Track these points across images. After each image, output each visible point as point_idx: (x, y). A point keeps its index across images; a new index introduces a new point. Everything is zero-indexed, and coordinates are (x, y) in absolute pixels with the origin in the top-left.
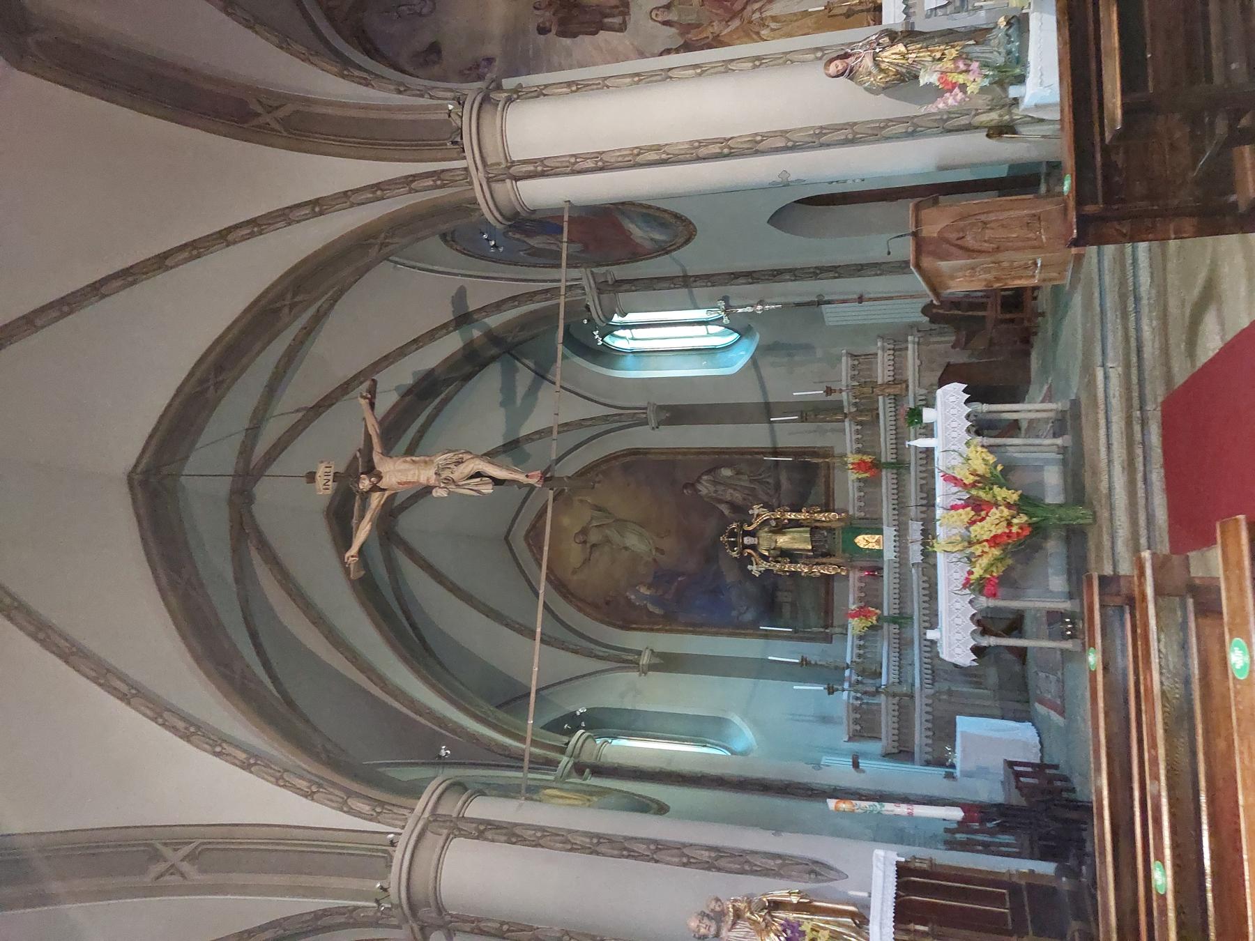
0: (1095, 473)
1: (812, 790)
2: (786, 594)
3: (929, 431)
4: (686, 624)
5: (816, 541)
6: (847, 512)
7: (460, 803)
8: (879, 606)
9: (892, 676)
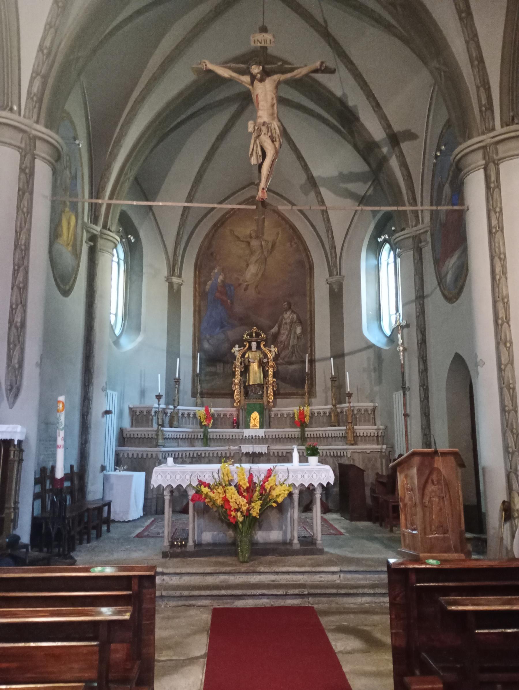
0: (271, 564)
1: (88, 386)
2: (222, 369)
3: (303, 459)
4: (199, 307)
5: (255, 387)
6: (274, 406)
7: (44, 155)
8: (214, 426)
9: (170, 434)
